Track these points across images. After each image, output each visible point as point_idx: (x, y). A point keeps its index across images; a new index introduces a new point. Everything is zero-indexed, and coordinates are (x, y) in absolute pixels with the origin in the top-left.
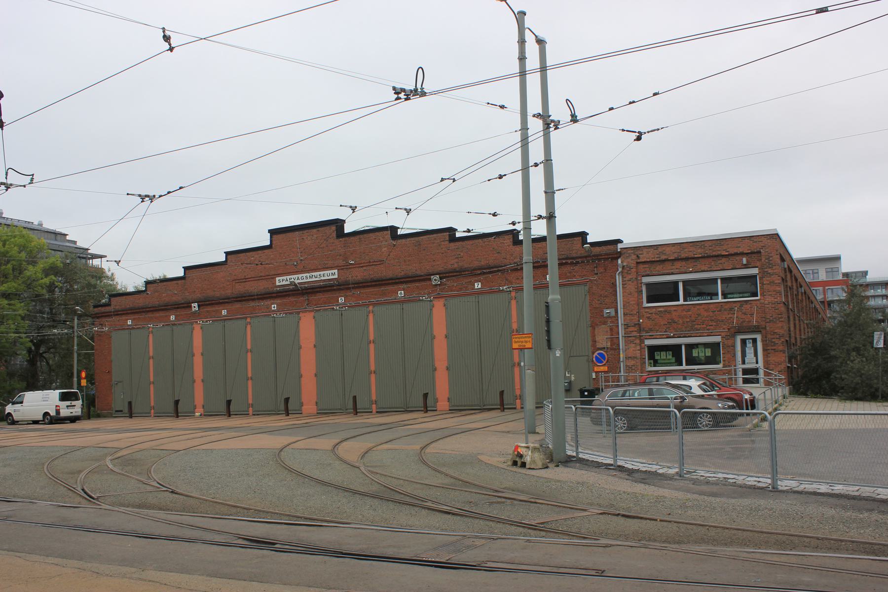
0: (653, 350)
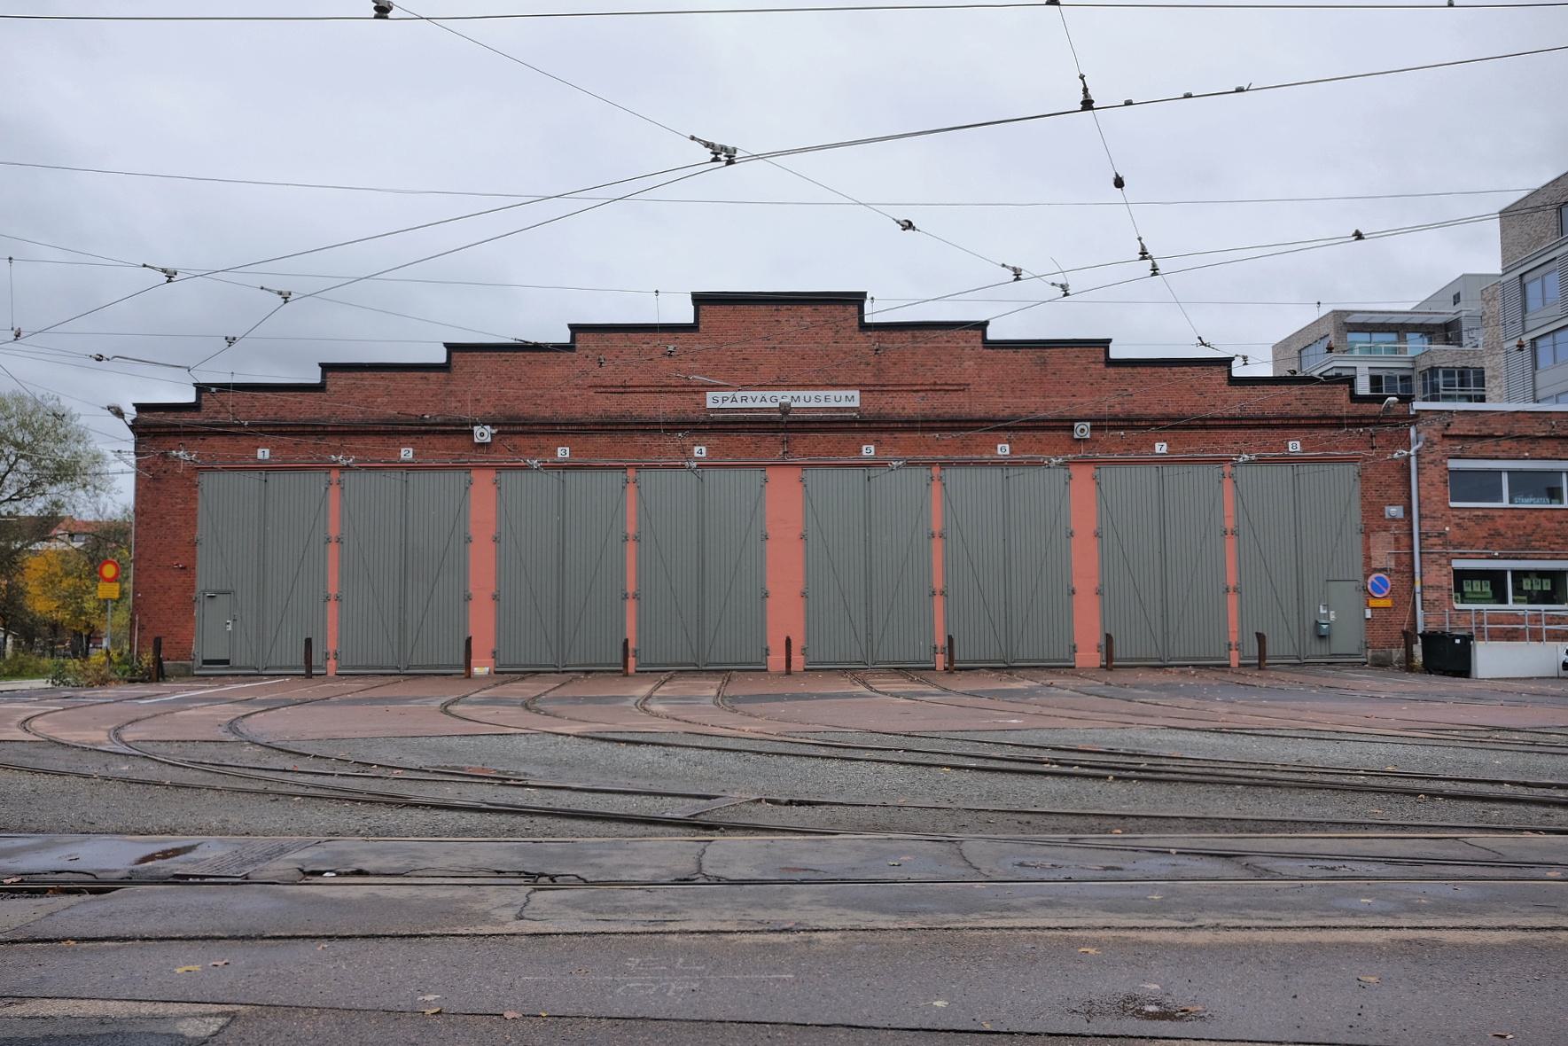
0: (1461, 576)
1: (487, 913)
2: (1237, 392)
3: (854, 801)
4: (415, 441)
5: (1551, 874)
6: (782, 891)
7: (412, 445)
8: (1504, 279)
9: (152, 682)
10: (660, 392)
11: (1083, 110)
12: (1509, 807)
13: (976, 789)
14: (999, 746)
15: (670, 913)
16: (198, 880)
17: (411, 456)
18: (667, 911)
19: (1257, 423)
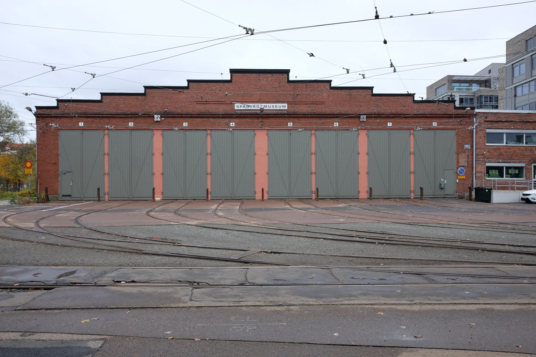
0: (489, 168)
1: (180, 298)
2: (416, 105)
3: (293, 252)
4: (134, 120)
5: (525, 281)
6: (275, 288)
7: (133, 121)
8: (506, 66)
9: (45, 203)
10: (219, 104)
11: (375, 19)
12: (508, 255)
13: (333, 247)
14: (338, 230)
15: (240, 298)
16: (79, 284)
17: (133, 125)
18: (239, 297)
19: (422, 116)
